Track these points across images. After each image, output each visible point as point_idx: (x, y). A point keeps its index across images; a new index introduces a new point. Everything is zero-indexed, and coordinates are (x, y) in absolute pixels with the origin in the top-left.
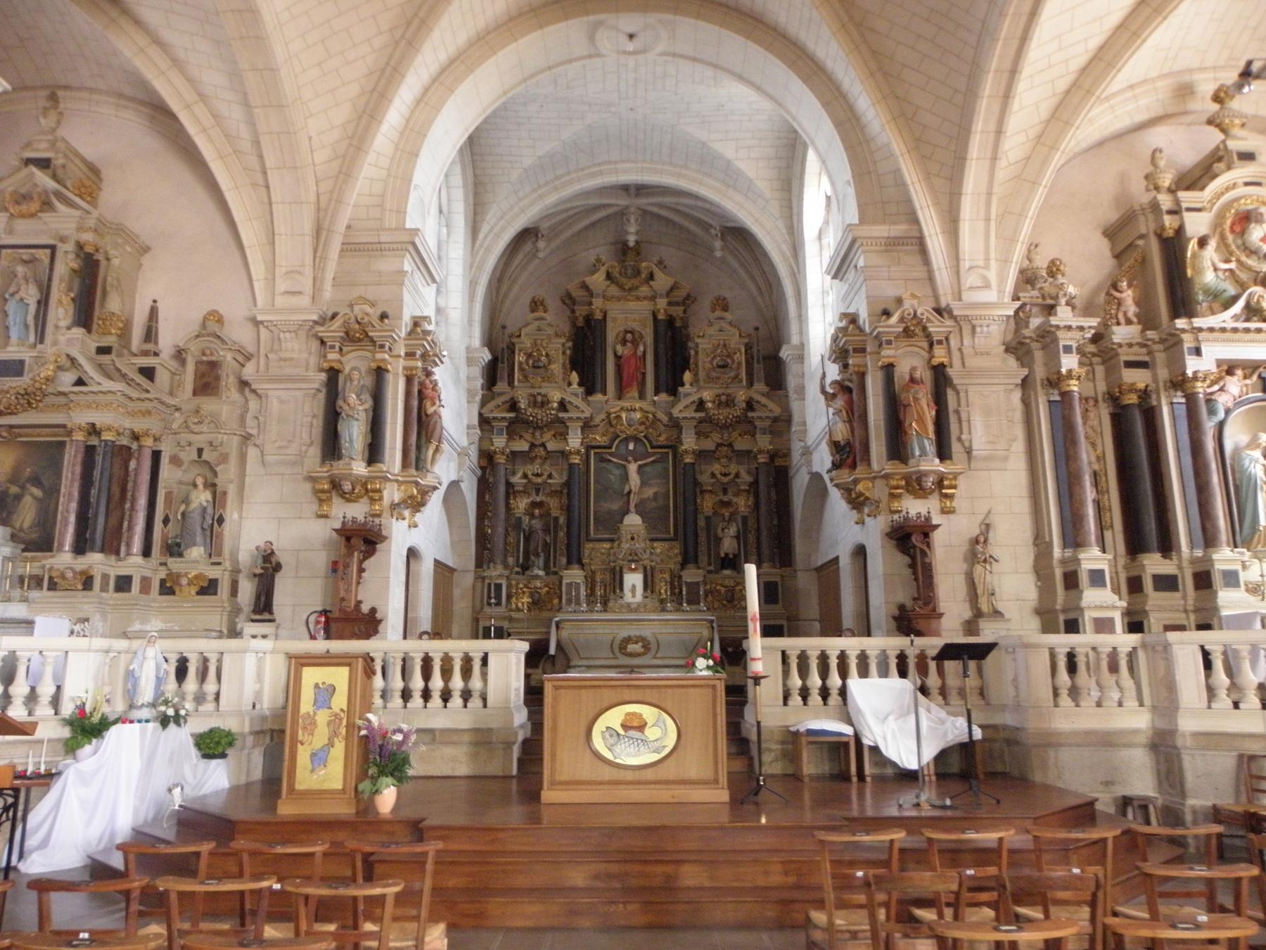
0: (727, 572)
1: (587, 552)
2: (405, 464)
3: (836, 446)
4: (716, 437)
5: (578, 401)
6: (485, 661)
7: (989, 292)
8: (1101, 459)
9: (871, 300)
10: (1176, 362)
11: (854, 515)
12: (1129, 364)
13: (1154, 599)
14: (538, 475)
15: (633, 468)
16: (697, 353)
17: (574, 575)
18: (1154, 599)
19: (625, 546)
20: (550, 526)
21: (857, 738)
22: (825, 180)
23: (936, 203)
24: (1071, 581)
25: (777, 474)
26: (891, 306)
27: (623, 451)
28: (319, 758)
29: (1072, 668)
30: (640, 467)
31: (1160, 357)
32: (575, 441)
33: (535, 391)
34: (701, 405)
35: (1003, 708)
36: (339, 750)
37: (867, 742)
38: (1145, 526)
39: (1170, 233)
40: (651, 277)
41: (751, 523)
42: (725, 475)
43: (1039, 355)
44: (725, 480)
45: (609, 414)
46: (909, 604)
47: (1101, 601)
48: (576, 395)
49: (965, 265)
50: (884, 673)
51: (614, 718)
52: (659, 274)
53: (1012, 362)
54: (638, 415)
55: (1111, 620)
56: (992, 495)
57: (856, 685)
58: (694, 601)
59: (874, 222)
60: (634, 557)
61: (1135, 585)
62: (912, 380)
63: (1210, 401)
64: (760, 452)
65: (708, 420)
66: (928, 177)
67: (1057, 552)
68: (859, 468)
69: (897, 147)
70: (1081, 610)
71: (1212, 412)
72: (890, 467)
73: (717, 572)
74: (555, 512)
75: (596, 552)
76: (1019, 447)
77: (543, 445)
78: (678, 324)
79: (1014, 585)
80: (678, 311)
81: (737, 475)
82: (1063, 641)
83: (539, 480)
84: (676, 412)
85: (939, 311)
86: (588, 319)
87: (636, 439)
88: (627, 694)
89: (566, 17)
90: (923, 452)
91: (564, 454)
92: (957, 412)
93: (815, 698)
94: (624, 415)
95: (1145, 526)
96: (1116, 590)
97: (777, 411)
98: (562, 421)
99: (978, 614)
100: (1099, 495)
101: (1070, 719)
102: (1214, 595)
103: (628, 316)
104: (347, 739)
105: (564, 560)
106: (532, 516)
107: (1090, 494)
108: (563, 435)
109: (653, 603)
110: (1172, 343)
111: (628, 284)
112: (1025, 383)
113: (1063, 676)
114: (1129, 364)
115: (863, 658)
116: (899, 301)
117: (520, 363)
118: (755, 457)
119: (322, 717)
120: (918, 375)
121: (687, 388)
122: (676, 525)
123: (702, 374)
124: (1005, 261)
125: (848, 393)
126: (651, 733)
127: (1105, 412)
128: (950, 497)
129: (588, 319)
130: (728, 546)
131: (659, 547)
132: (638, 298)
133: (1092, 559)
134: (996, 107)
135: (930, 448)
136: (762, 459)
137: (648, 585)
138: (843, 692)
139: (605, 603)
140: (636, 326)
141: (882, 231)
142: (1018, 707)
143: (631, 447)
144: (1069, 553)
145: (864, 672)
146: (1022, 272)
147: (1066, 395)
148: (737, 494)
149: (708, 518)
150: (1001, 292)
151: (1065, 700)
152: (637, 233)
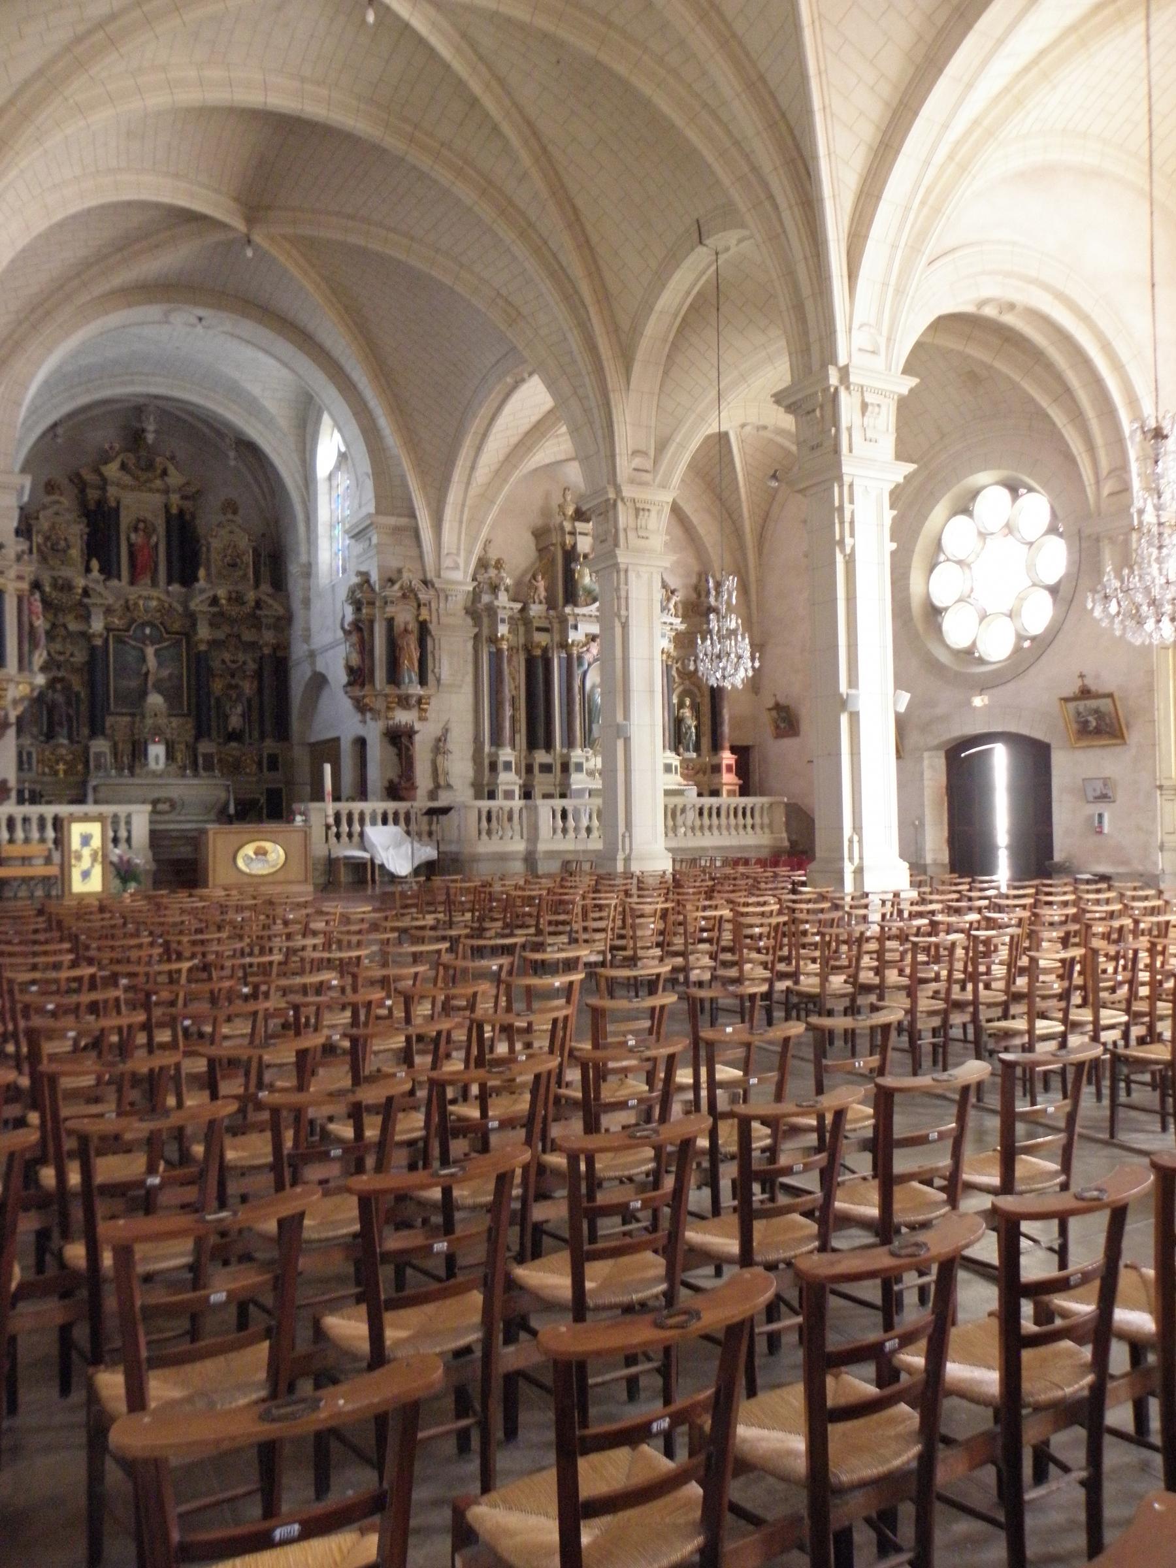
0: (234, 744)
1: (108, 724)
2: (21, 668)
3: (350, 670)
4: (227, 629)
5: (100, 588)
6: (129, 816)
7: (459, 576)
8: (517, 688)
9: (381, 568)
10: (564, 633)
11: (359, 717)
12: (539, 629)
13: (539, 778)
14: (60, 653)
15: (150, 651)
16: (208, 550)
17: (100, 746)
18: (539, 778)
19: (149, 722)
20: (71, 698)
21: (372, 860)
22: (337, 436)
23: (429, 505)
24: (493, 767)
25: (277, 666)
26: (394, 577)
27: (139, 633)
28: (86, 875)
29: (489, 819)
30: (156, 651)
31: (556, 626)
32: (97, 625)
33: (56, 574)
34: (214, 601)
35: (451, 842)
36: (97, 871)
37: (378, 862)
38: (538, 735)
39: (569, 547)
40: (165, 473)
41: (255, 704)
42: (233, 662)
43: (485, 620)
44: (234, 666)
45: (127, 601)
46: (396, 780)
47: (509, 780)
48: (97, 582)
49: (444, 551)
50: (385, 822)
51: (249, 850)
52: (171, 469)
53: (469, 621)
54: (154, 603)
55: (541, 771)
56: (451, 710)
57: (369, 830)
58: (209, 767)
59: (386, 514)
60: (157, 731)
61: (529, 769)
62: (406, 630)
63: (580, 658)
64: (267, 645)
65: (222, 614)
66: (424, 487)
67: (487, 748)
68: (367, 687)
69: (406, 465)
70: (497, 785)
71: (580, 664)
72: (389, 689)
73: (225, 744)
74: (77, 687)
75: (117, 722)
76: (469, 678)
77: (65, 626)
78: (188, 517)
79: (460, 768)
80: (188, 505)
81: (244, 663)
82: (485, 804)
83: (62, 658)
84: (193, 606)
85: (425, 582)
86: (100, 503)
87: (150, 624)
88: (256, 836)
89: (150, 302)
90: (411, 681)
91: (84, 634)
92: (433, 653)
93: (345, 838)
94: (141, 602)
95: (538, 735)
96: (518, 772)
97: (281, 611)
98: (86, 607)
99: (437, 786)
100: (514, 713)
101: (486, 846)
102: (569, 777)
103: (140, 505)
104: (103, 863)
105: (85, 731)
106: (55, 691)
107: (508, 712)
108: (86, 618)
109: (174, 768)
110: (563, 620)
111: (144, 476)
112: (476, 637)
113: (484, 823)
114: (539, 629)
115: (396, 814)
116: (400, 571)
117: (38, 546)
118: (261, 648)
119: (86, 852)
120: (410, 627)
121: (202, 584)
122: (189, 705)
123: (213, 570)
124: (470, 552)
125: (360, 631)
126: (272, 857)
127: (522, 657)
128: (425, 710)
129: (100, 503)
130: (235, 721)
131: (175, 722)
132: (151, 490)
133: (507, 754)
134: (472, 454)
135: (415, 678)
136: (266, 651)
137: (170, 756)
138: (362, 835)
139: (131, 769)
140: (149, 516)
141: (392, 521)
142: (459, 841)
143: (148, 631)
144: (493, 749)
145: (374, 823)
146: (480, 560)
147: (499, 651)
148: (244, 678)
149: (218, 700)
150: (465, 572)
151: (484, 836)
152: (156, 431)
